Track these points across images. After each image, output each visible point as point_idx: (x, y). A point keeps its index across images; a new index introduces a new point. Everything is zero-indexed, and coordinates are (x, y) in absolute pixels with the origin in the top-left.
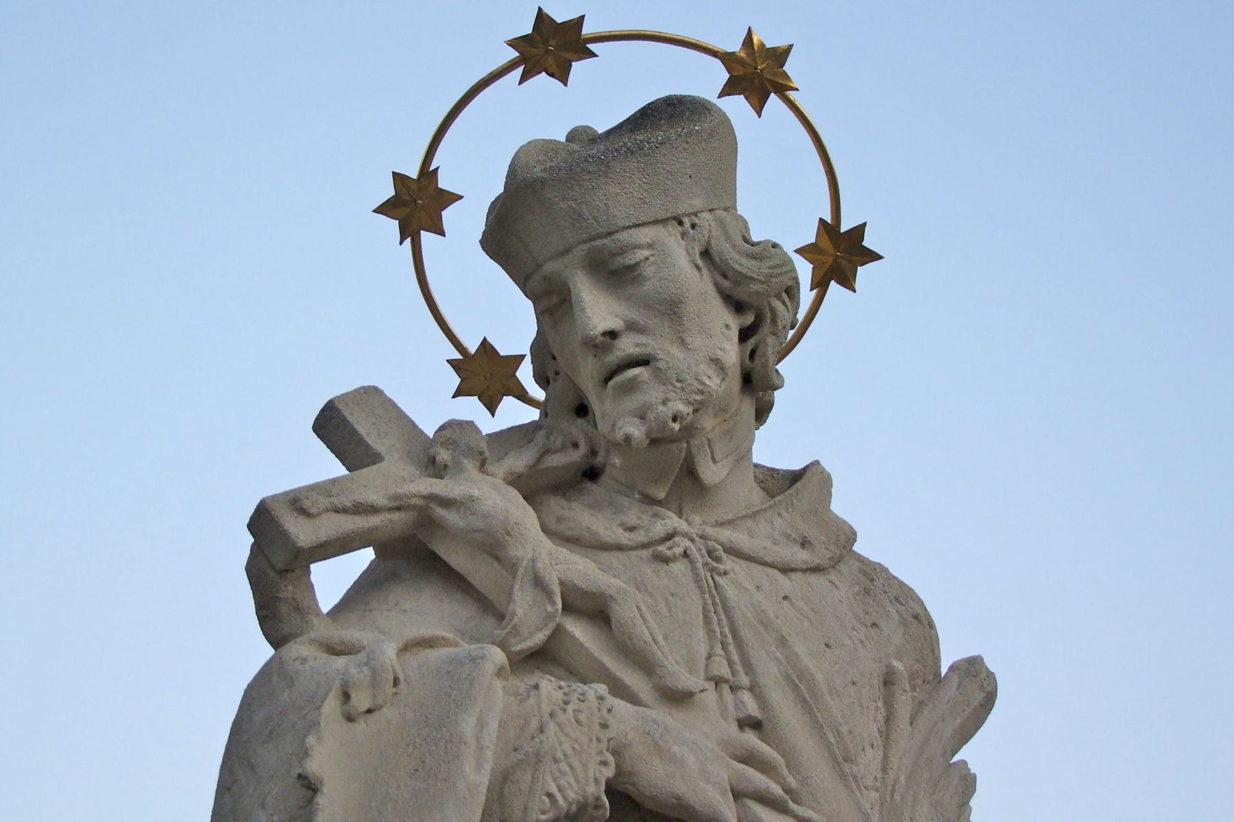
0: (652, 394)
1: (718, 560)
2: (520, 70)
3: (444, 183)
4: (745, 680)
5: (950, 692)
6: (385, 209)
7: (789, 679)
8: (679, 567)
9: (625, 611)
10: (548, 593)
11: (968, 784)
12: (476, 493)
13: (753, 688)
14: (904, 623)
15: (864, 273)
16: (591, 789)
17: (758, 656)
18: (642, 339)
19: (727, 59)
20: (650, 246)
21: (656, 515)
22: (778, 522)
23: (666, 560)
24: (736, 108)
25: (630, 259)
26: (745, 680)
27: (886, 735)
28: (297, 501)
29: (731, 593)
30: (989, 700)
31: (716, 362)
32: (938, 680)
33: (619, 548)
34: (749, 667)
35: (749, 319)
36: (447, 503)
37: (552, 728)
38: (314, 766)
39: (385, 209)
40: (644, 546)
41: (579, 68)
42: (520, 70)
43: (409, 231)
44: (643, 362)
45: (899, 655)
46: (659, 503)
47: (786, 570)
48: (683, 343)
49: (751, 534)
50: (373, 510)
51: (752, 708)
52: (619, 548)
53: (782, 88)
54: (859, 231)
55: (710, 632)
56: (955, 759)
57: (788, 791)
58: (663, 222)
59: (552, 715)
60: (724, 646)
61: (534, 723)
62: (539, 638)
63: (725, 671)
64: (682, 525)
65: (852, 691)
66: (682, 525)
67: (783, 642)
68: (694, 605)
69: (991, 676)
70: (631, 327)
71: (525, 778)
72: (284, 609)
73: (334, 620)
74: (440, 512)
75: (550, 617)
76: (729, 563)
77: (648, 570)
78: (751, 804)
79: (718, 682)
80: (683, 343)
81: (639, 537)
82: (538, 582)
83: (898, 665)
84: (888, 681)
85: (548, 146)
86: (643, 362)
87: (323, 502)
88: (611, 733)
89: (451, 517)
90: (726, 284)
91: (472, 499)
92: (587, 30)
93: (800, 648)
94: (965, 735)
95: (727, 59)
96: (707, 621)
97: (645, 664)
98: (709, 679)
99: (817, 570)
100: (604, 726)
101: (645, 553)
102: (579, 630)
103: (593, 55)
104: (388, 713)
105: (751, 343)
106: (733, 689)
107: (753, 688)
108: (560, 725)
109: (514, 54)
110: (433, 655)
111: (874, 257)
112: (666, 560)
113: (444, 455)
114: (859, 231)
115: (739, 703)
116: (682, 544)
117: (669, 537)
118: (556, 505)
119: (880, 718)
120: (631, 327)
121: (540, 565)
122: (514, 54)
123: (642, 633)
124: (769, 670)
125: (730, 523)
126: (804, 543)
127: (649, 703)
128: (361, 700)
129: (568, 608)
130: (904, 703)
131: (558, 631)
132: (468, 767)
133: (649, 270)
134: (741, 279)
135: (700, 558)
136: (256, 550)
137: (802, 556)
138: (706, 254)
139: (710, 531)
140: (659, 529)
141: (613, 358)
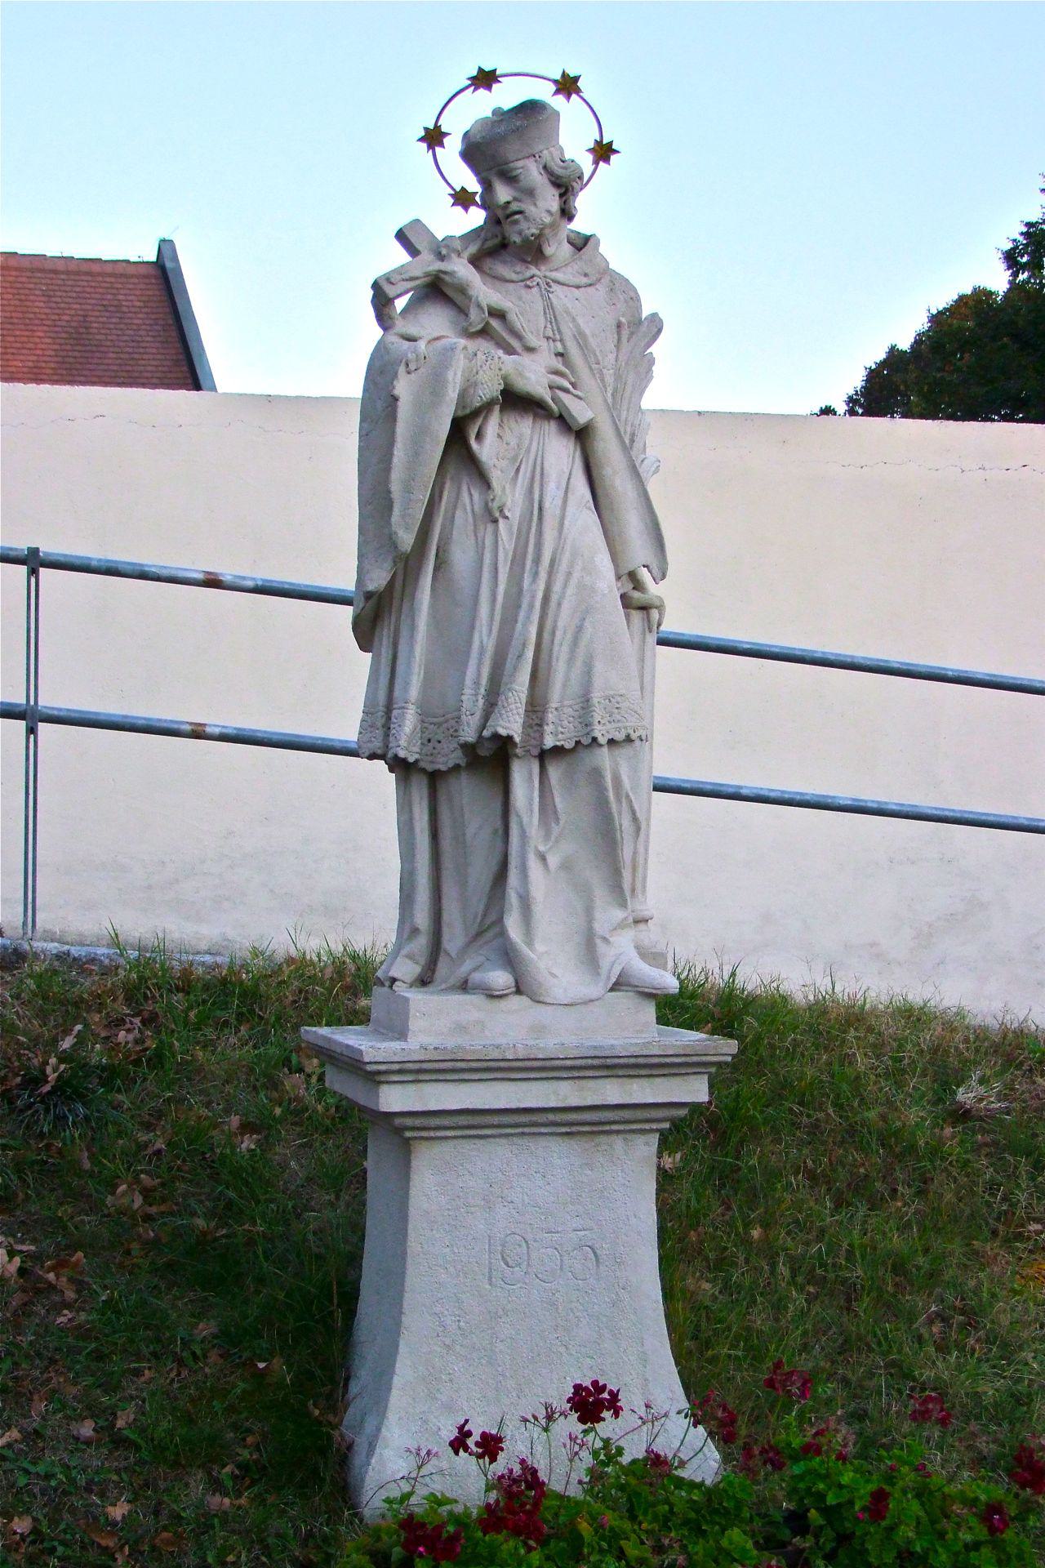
0: (523, 225)
1: (550, 287)
2: (473, 88)
3: (444, 129)
4: (558, 337)
5: (644, 329)
6: (421, 140)
7: (574, 336)
8: (535, 290)
9: (512, 317)
10: (482, 309)
11: (652, 362)
12: (456, 269)
13: (561, 340)
14: (626, 301)
15: (613, 158)
16: (495, 394)
17: (564, 329)
18: (519, 204)
19: (555, 82)
20: (522, 168)
21: (527, 268)
22: (576, 267)
23: (529, 287)
24: (558, 103)
25: (514, 173)
26: (558, 337)
27: (618, 346)
28: (388, 278)
29: (554, 300)
30: (660, 331)
31: (549, 211)
32: (640, 322)
33: (513, 282)
34: (560, 332)
35: (563, 190)
36: (445, 273)
37: (481, 372)
38: (396, 392)
39: (421, 140)
40: (522, 281)
41: (495, 86)
42: (473, 88)
43: (431, 147)
44: (520, 212)
45: (623, 316)
46: (529, 263)
47: (578, 287)
48: (535, 204)
49: (564, 273)
50: (417, 278)
51: (560, 349)
52: (513, 282)
53: (578, 91)
54: (611, 143)
55: (546, 318)
56: (648, 351)
57: (572, 384)
58: (528, 157)
59: (481, 367)
60: (551, 323)
61: (475, 371)
62: (479, 327)
63: (551, 334)
64: (537, 273)
65: (602, 334)
66: (537, 273)
67: (574, 320)
68: (539, 306)
69: (661, 321)
70: (515, 199)
71: (472, 391)
72: (385, 318)
73: (404, 318)
74: (442, 276)
75: (483, 319)
76: (555, 287)
77: (523, 292)
78: (557, 391)
79: (548, 338)
80: (535, 204)
81: (520, 277)
82: (479, 306)
83: (623, 320)
84: (619, 326)
85: (484, 121)
86: (520, 212)
87: (399, 277)
88: (503, 372)
89: (447, 278)
90: (553, 179)
91: (454, 272)
92: (498, 73)
93: (580, 321)
94: (650, 344)
95: (555, 82)
96: (545, 313)
97: (518, 336)
98: (544, 337)
99: (590, 285)
100: (500, 369)
101: (522, 284)
102: (495, 324)
103: (499, 82)
104: (422, 370)
105: (564, 198)
106: (554, 341)
107: (561, 340)
108: (484, 371)
109: (470, 82)
110: (439, 344)
111: (616, 152)
112: (529, 287)
113: (444, 252)
114: (611, 143)
115: (556, 347)
116: (537, 280)
117: (532, 277)
118: (488, 263)
119: (616, 341)
120: (515, 199)
121: (479, 299)
122: (470, 82)
123: (518, 325)
124: (568, 331)
125: (556, 270)
126: (586, 275)
127: (520, 351)
128: (412, 367)
129: (490, 314)
130: (625, 333)
131: (487, 323)
132: (450, 392)
133: (522, 177)
134: (558, 177)
135: (543, 286)
136: (374, 296)
137: (584, 280)
138: (545, 167)
139: (548, 274)
140: (528, 274)
141: (508, 212)
